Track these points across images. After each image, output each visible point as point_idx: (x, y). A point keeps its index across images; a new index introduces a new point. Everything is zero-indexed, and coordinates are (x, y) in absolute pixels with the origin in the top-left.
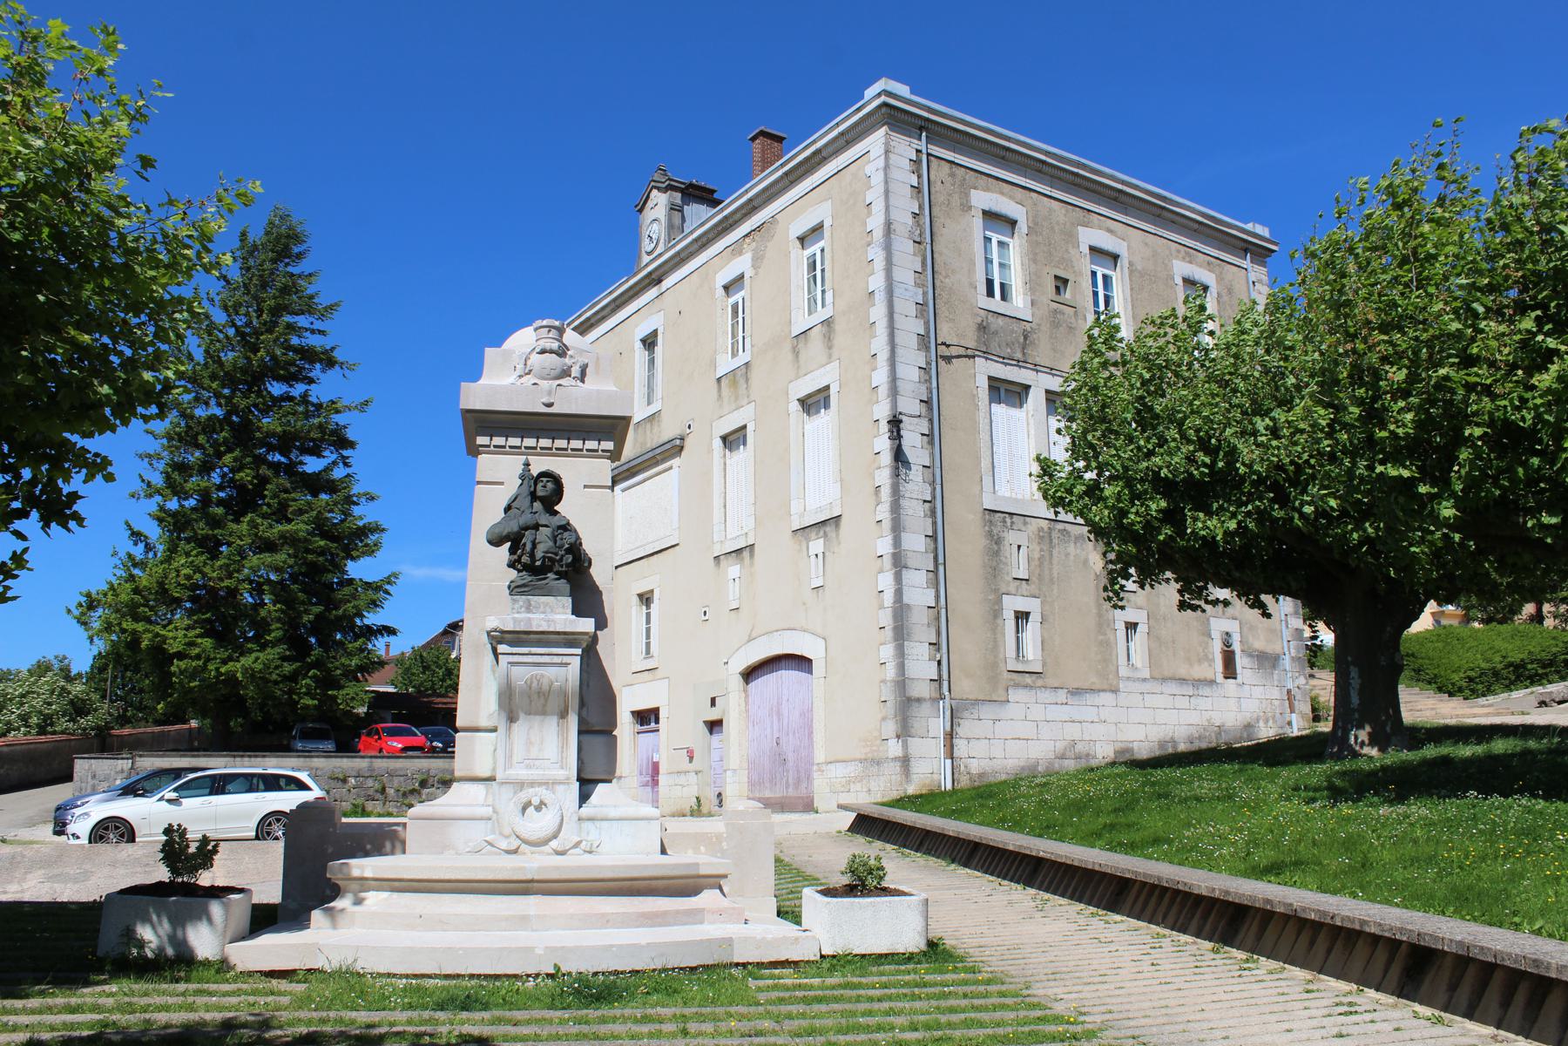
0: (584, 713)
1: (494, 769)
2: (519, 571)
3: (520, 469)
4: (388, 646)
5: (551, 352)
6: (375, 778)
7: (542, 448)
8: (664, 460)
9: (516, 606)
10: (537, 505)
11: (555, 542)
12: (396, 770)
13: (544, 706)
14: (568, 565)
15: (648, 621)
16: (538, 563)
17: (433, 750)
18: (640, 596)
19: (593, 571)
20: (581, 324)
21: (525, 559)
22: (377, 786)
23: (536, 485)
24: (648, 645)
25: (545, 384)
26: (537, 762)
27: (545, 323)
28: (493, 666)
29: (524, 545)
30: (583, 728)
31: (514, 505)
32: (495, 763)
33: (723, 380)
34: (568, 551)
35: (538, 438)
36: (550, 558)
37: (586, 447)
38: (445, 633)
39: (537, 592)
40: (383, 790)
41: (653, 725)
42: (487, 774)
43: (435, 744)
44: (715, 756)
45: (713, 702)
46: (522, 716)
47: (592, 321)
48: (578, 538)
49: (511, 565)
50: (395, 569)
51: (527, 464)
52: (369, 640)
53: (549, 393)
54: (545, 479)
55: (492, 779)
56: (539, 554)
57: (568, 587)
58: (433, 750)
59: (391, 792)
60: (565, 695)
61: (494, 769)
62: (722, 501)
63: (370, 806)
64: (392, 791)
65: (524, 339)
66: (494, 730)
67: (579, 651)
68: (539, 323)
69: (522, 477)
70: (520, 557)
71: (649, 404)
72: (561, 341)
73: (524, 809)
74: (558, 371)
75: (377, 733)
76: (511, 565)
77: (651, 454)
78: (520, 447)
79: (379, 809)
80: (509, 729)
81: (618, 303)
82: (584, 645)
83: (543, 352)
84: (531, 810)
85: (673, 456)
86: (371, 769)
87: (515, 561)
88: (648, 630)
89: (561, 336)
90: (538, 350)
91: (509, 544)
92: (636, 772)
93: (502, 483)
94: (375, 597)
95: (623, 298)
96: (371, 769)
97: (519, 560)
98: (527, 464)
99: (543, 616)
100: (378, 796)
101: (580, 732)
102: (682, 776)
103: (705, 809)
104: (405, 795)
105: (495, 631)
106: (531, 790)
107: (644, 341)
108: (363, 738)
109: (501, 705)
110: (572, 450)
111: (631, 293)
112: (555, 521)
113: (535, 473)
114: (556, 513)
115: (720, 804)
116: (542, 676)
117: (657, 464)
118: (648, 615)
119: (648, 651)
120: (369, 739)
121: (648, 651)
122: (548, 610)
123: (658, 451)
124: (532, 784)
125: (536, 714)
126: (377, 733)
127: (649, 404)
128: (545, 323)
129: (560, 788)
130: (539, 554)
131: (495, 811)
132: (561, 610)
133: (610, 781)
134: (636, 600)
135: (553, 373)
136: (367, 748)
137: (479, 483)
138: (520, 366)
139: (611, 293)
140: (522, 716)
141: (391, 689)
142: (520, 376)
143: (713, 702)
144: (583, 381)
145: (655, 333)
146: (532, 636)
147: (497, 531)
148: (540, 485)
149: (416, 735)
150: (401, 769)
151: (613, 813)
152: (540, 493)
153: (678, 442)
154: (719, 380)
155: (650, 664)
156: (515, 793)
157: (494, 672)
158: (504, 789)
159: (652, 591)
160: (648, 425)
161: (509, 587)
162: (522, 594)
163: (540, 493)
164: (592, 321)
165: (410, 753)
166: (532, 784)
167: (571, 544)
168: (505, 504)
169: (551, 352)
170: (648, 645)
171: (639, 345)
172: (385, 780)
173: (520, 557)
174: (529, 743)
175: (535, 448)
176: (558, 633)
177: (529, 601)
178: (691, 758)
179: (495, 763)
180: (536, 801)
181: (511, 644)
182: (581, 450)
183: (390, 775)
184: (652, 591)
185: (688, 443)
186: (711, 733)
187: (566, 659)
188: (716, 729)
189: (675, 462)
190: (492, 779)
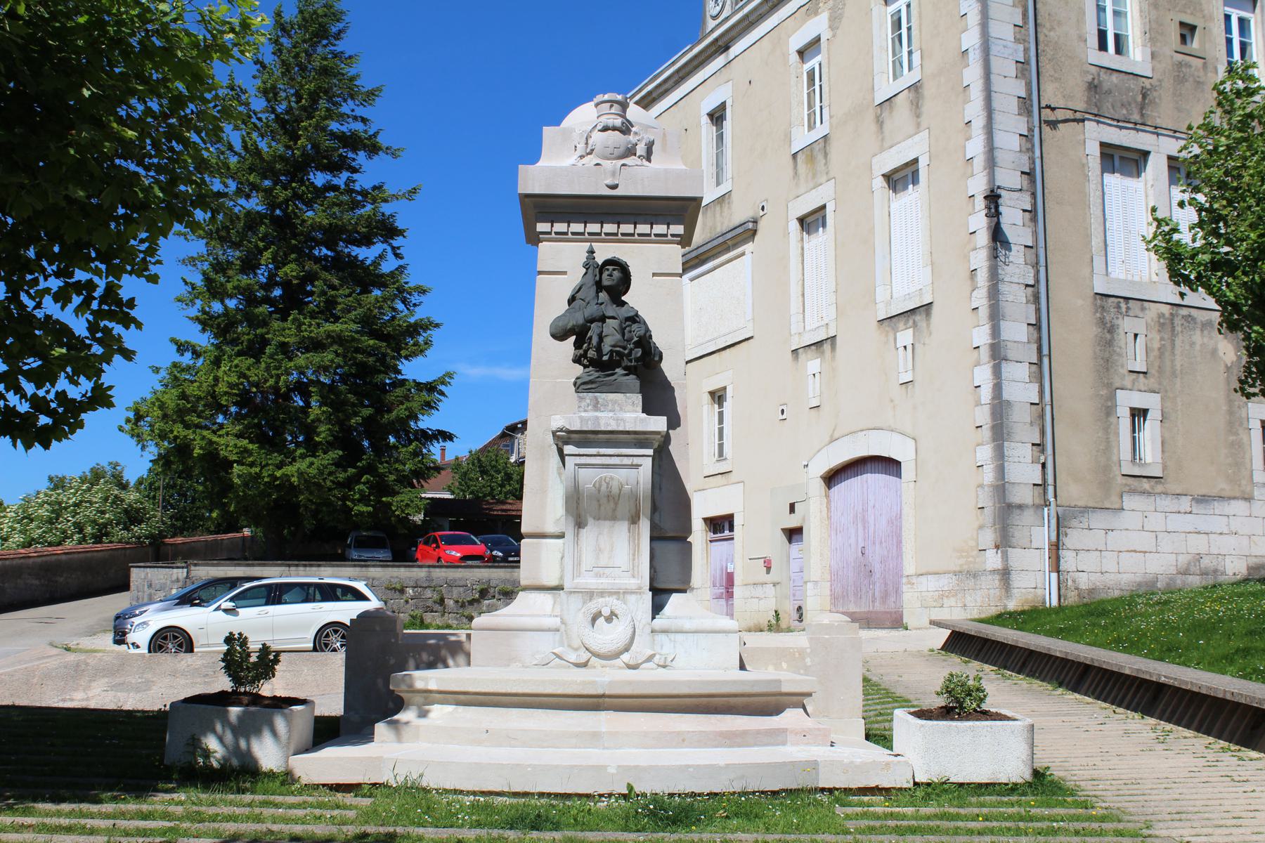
0: (657, 515)
1: (562, 578)
2: (585, 367)
3: (583, 257)
4: (443, 450)
5: (614, 129)
6: (434, 588)
7: (606, 234)
8: (735, 246)
9: (583, 404)
10: (603, 296)
11: (623, 335)
12: (455, 581)
13: (614, 510)
14: (637, 360)
15: (721, 421)
16: (605, 358)
17: (493, 559)
18: (712, 394)
19: (665, 366)
20: (643, 98)
21: (591, 353)
22: (436, 597)
23: (601, 274)
24: (721, 446)
25: (608, 164)
26: (607, 570)
27: (606, 97)
28: (558, 469)
29: (591, 338)
30: (655, 535)
31: (578, 296)
32: (562, 571)
33: (799, 156)
34: (637, 345)
35: (602, 223)
36: (618, 353)
37: (654, 231)
38: (503, 435)
39: (605, 388)
40: (441, 601)
41: (727, 533)
42: (553, 582)
43: (494, 553)
44: (795, 566)
45: (792, 508)
46: (591, 521)
47: (654, 95)
48: (648, 330)
49: (577, 360)
50: (450, 368)
51: (591, 252)
52: (424, 445)
53: (613, 174)
54: (611, 268)
55: (559, 588)
56: (606, 348)
57: (638, 383)
58: (493, 559)
59: (450, 603)
60: (637, 499)
61: (562, 578)
62: (800, 289)
63: (428, 618)
64: (452, 602)
66: (561, 536)
67: (650, 452)
68: (600, 98)
69: (586, 266)
70: (586, 352)
71: (718, 184)
72: (624, 117)
73: (594, 620)
74: (622, 149)
75: (435, 541)
76: (577, 360)
77: (721, 240)
78: (583, 234)
79: (439, 622)
80: (577, 535)
81: (681, 74)
82: (656, 445)
83: (605, 129)
84: (601, 620)
85: (745, 241)
86: (429, 579)
87: (581, 356)
88: (721, 431)
89: (624, 110)
90: (599, 127)
91: (574, 337)
92: (709, 584)
93: (564, 273)
94: (429, 399)
95: (687, 70)
96: (429, 579)
97: (585, 355)
98: (591, 252)
99: (611, 414)
100: (437, 607)
101: (652, 539)
102: (760, 587)
103: (783, 624)
104: (463, 606)
105: (561, 430)
106: (601, 600)
107: (711, 115)
108: (421, 546)
109: (567, 510)
110: (639, 235)
111: (695, 63)
112: (623, 312)
113: (600, 260)
114: (624, 303)
115: (800, 619)
116: (612, 478)
117: (728, 250)
118: (721, 414)
119: (721, 453)
120: (427, 548)
121: (721, 453)
122: (617, 408)
123: (729, 236)
124: (602, 594)
125: (605, 519)
126: (435, 541)
127: (718, 184)
128: (606, 97)
129: (632, 599)
130: (606, 348)
131: (563, 622)
132: (630, 407)
133: (684, 591)
134: (707, 397)
135: (617, 152)
136: (425, 557)
137: (540, 273)
138: (581, 146)
139: (673, 63)
140: (591, 521)
141: (448, 496)
142: (582, 157)
143: (792, 508)
144: (649, 160)
145: (723, 106)
146: (600, 436)
148: (605, 275)
149: (475, 543)
150: (460, 579)
151: (688, 625)
152: (606, 281)
153: (750, 225)
154: (795, 156)
155: (723, 467)
156: (584, 603)
157: (560, 474)
158: (573, 598)
159: (725, 388)
160: (718, 208)
161: (575, 384)
162: (588, 390)
163: (606, 281)
164: (654, 95)
165: (470, 563)
166: (602, 594)
167: (640, 337)
168: (568, 295)
169: (614, 129)
170: (721, 446)
171: (705, 120)
172: (444, 591)
173: (586, 352)
174: (599, 550)
175: (599, 234)
176: (628, 433)
177: (596, 398)
178: (768, 569)
179: (562, 571)
180: (606, 612)
181: (579, 444)
182: (649, 235)
183: (450, 586)
184: (725, 388)
185: (762, 226)
186: (790, 541)
187: (636, 461)
188: (795, 537)
189: (748, 247)
190: (559, 588)
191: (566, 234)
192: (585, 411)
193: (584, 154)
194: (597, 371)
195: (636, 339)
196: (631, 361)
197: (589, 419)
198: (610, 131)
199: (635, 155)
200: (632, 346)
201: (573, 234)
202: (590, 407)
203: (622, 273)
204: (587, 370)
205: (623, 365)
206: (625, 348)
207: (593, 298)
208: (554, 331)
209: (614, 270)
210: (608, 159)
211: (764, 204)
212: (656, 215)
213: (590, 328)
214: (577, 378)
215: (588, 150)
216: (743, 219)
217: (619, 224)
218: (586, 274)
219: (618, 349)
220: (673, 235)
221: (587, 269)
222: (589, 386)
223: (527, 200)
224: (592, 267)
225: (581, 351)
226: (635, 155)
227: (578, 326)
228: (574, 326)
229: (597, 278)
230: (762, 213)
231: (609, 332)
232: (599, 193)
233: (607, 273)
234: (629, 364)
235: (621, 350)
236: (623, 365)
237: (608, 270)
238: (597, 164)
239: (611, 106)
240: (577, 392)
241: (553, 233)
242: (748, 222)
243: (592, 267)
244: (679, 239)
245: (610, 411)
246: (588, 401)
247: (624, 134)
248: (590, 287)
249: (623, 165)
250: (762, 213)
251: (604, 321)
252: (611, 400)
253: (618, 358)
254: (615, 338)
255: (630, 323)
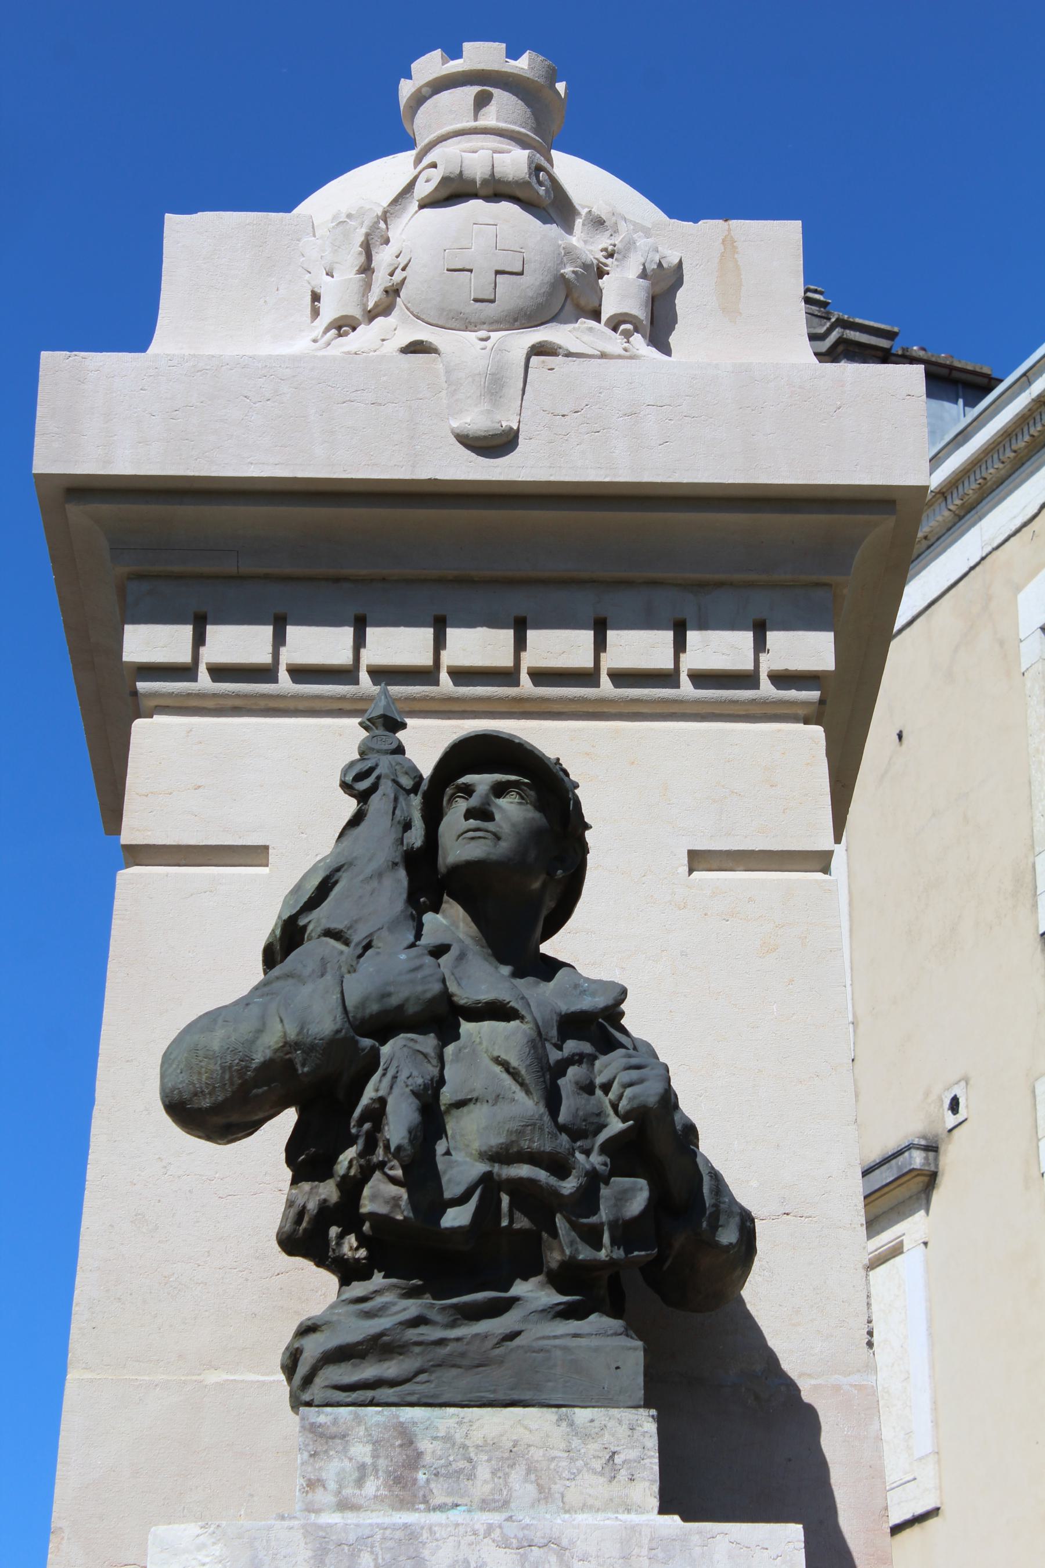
7: (461, 675)
9: (333, 1468)
11: (553, 1100)
16: (456, 1218)
23: (433, 815)
29: (377, 1113)
31: (317, 920)
36: (519, 1189)
39: (453, 1382)
54: (482, 781)
65: (581, 1257)
74: (533, 282)
87: (326, 1214)
90: (424, 189)
91: (288, 1119)
114: (550, 968)
132: (594, 1486)
142: (343, 326)
144: (659, 337)
147: (216, 1040)
153: (917, 1159)
161: (291, 1364)
173: (352, 1188)
177: (407, 1437)
191: (265, 673)
192: (344, 1505)
193: (356, 312)
194: (411, 1293)
195: (616, 1126)
196: (592, 1237)
197: (364, 1541)
198: (475, 205)
199: (596, 315)
200: (597, 1160)
201: (300, 673)
202: (372, 1487)
203: (540, 806)
204: (358, 1289)
205: (554, 1258)
206: (560, 1167)
207: (393, 926)
208: (181, 1080)
209: (500, 790)
210: (468, 325)
211: (959, 1091)
212: (700, 587)
213: (371, 1064)
214: (307, 1329)
215: (375, 296)
216: (891, 1145)
217: (520, 627)
218: (356, 820)
219: (524, 1171)
220: (781, 679)
221: (363, 797)
222: (369, 1371)
223: (77, 512)
224: (386, 787)
225: (328, 1191)
226: (596, 315)
227: (308, 1048)
228: (289, 1046)
229: (416, 837)
230: (951, 1120)
231: (477, 1086)
232: (423, 473)
233: (462, 805)
234: (585, 1253)
235: (542, 1175)
236: (554, 1258)
237: (468, 791)
238: (416, 348)
239: (482, 101)
240: (297, 1403)
241: (203, 671)
242: (909, 1147)
243: (386, 787)
244: (814, 695)
245: (485, 1505)
246: (362, 1451)
247: (546, 219)
248: (379, 875)
249: (540, 350)
250: (951, 1120)
251: (448, 1034)
252: (490, 1446)
253: (522, 1223)
254: (504, 1110)
255: (586, 1047)
